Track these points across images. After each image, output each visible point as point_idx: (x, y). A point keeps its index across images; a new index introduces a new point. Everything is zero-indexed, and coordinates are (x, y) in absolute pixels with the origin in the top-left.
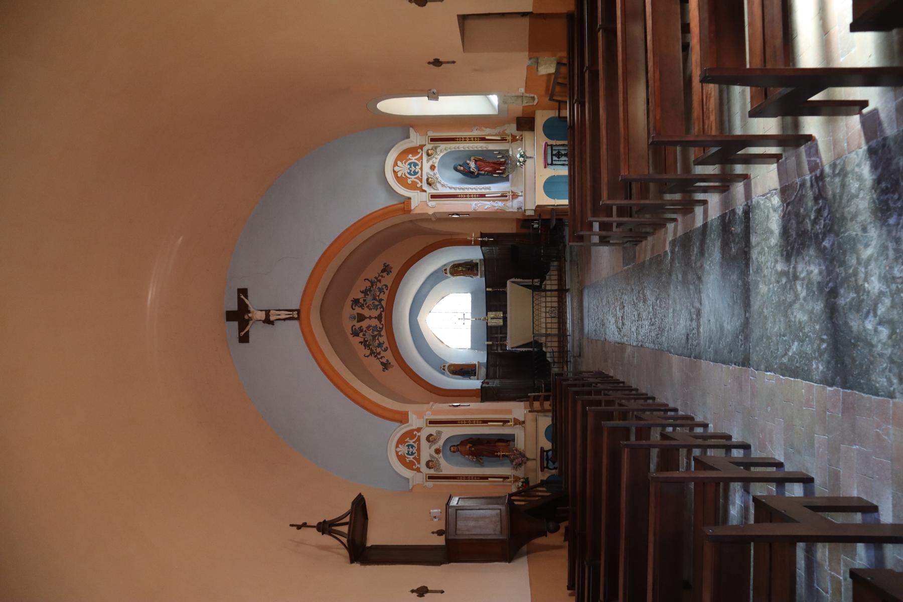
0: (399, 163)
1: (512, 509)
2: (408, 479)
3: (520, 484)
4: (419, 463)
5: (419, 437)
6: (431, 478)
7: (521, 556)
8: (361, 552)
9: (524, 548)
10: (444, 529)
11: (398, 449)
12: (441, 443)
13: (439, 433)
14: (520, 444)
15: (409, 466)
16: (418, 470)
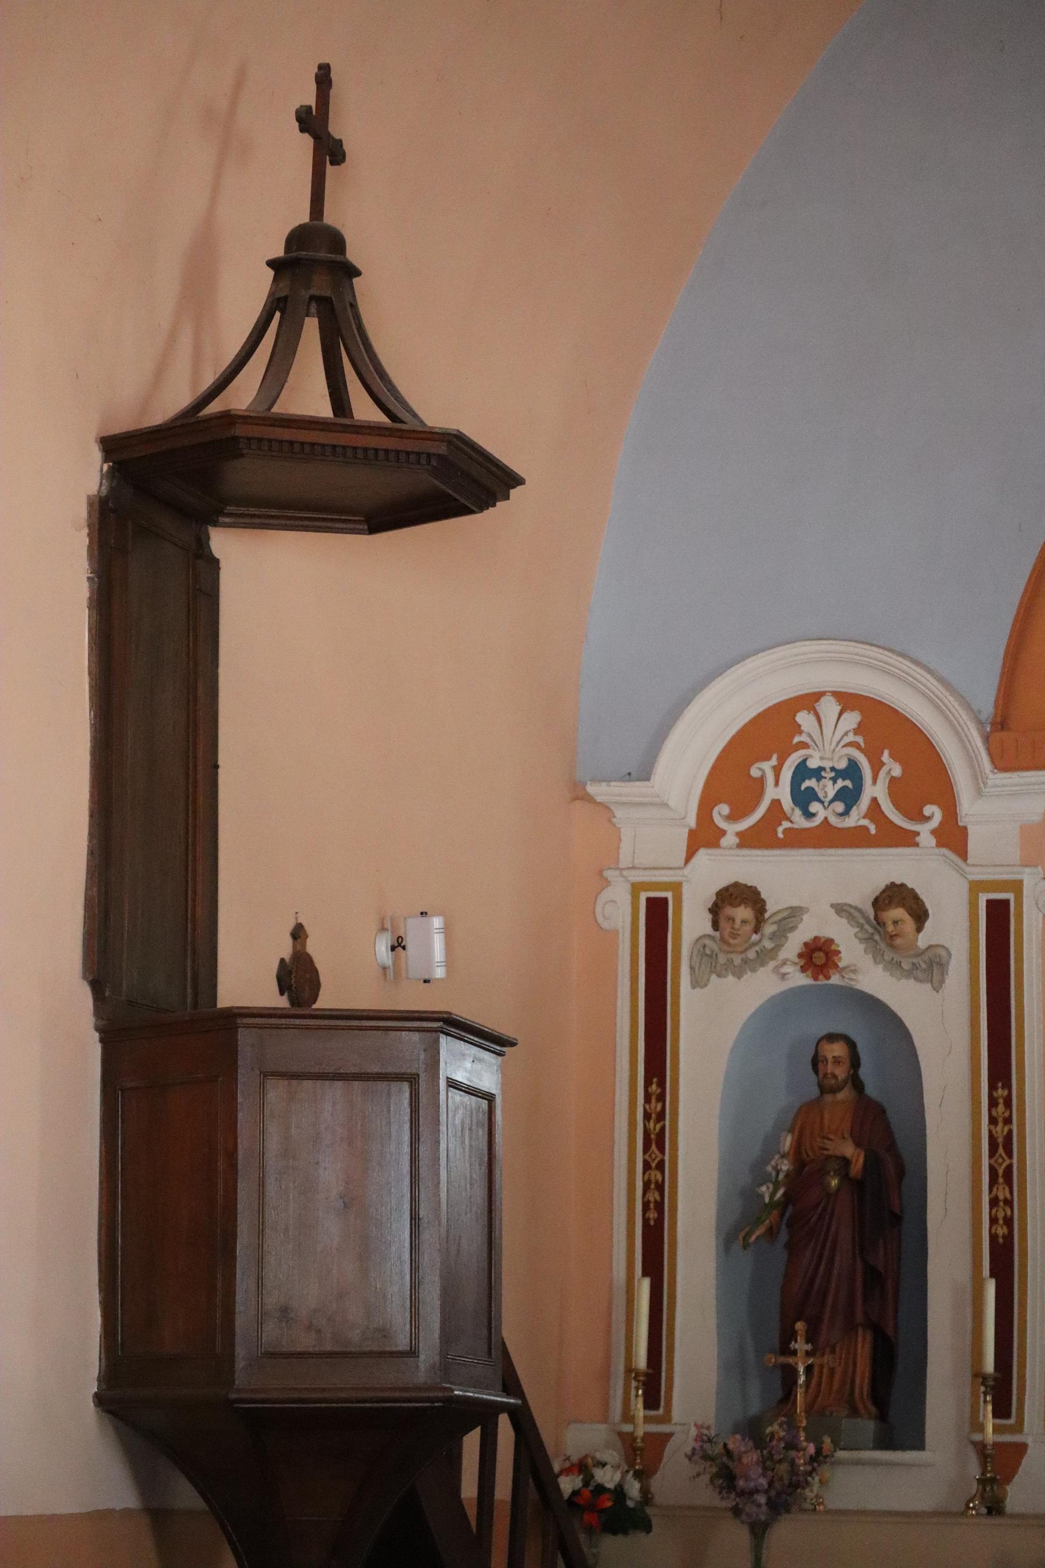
0: (852, 719)
1: (431, 1425)
2: (645, 775)
3: (608, 1478)
4: (748, 840)
5: (908, 839)
6: (657, 915)
7: (144, 1478)
8: (168, 497)
9: (186, 1496)
10: (325, 1001)
11: (829, 708)
12: (874, 979)
13: (931, 967)
14: (866, 1482)
15: (730, 779)
16: (703, 837)
